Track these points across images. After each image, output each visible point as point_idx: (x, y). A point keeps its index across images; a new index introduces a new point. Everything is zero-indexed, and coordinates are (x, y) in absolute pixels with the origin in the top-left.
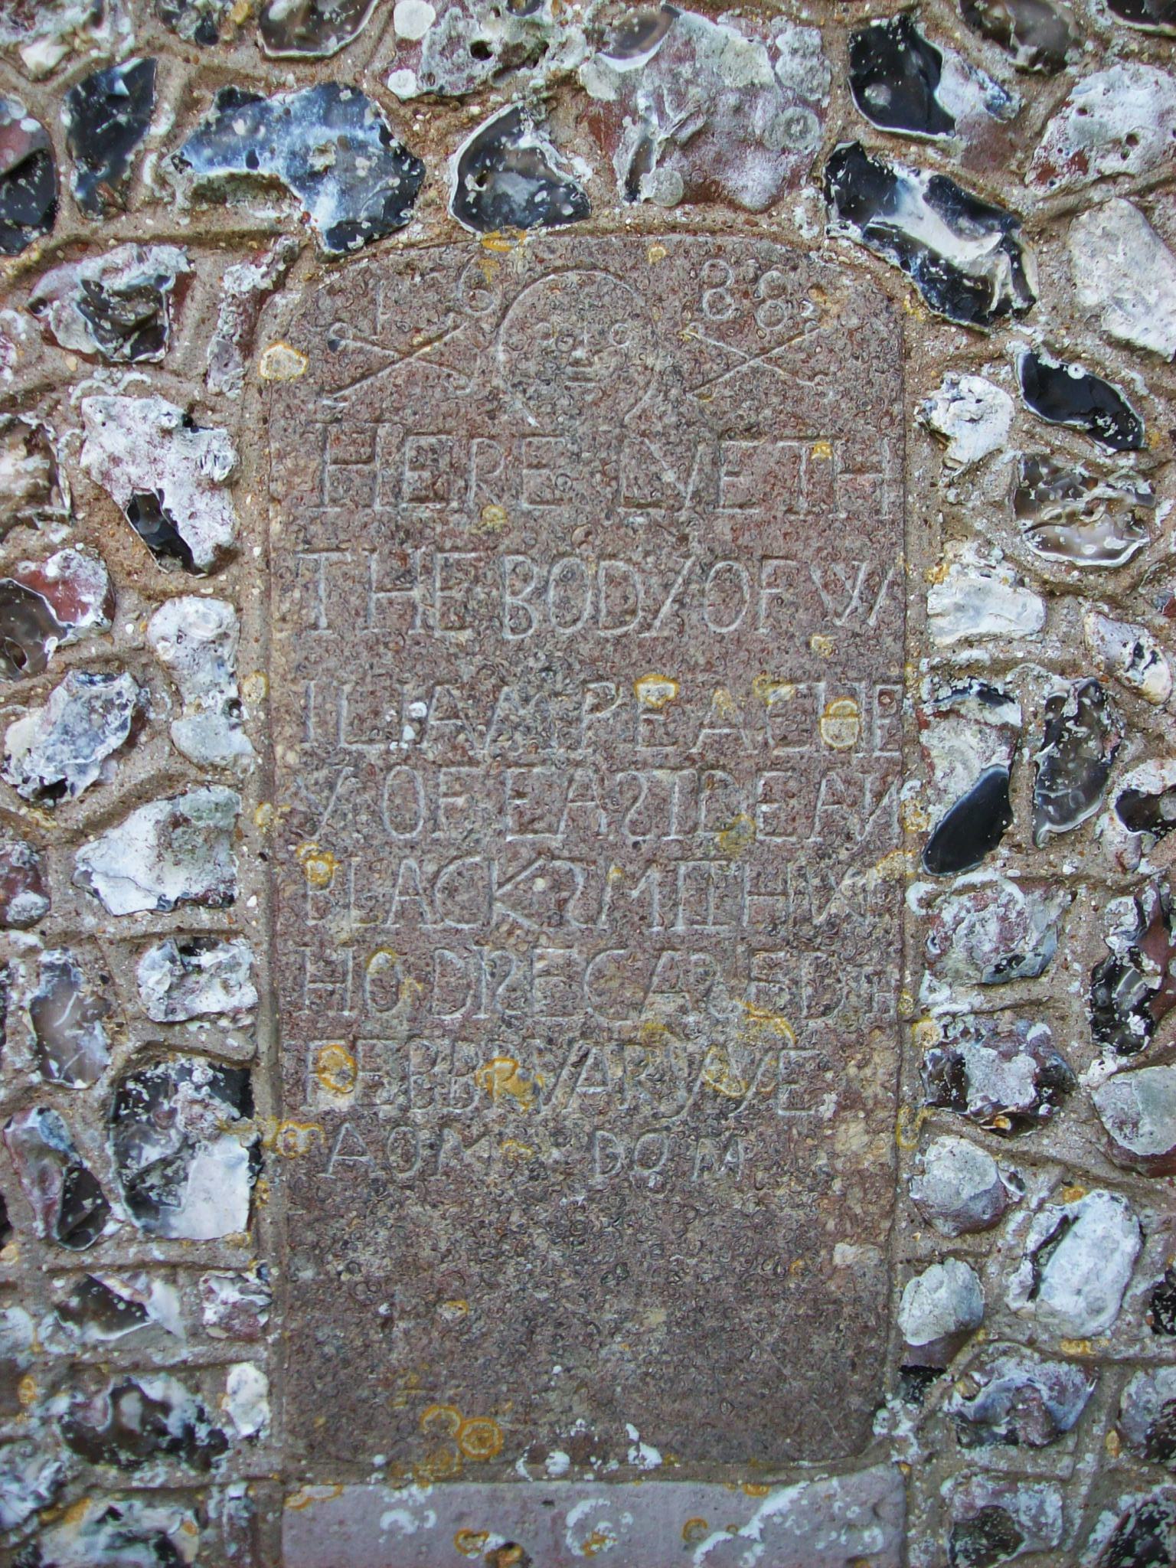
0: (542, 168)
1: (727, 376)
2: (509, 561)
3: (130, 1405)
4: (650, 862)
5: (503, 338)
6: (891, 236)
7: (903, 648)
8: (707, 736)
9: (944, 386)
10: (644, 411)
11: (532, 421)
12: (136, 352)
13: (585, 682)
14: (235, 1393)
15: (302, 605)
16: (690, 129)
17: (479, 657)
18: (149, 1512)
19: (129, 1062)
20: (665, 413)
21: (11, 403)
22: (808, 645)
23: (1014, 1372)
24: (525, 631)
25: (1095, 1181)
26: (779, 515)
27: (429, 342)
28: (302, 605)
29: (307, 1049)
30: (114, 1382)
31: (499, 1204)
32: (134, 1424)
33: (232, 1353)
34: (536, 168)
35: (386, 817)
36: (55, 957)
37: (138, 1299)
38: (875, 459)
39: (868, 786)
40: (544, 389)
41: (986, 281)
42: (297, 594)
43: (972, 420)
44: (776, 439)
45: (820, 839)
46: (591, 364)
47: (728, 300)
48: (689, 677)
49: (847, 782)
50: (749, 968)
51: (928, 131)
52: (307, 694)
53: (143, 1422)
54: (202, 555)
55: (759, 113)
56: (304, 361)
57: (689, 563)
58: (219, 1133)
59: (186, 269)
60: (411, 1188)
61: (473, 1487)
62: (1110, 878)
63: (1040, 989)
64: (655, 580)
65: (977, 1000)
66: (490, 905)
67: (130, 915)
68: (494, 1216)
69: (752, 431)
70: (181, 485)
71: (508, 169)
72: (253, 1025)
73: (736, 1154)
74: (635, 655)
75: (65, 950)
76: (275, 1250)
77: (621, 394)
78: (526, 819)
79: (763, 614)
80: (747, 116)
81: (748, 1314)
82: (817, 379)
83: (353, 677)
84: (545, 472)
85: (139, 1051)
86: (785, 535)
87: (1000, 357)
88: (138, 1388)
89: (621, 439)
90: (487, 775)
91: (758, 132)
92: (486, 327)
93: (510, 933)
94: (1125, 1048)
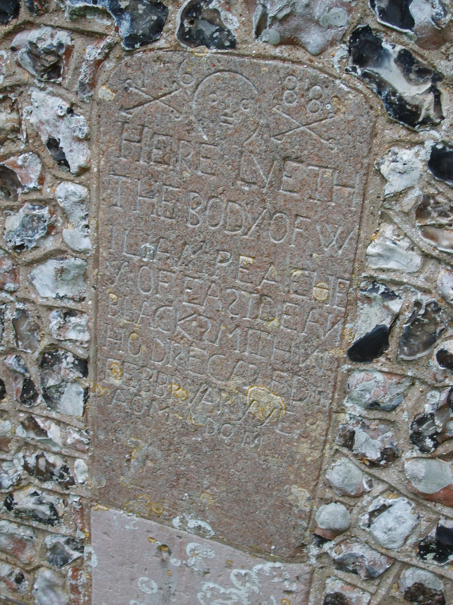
0: (218, 20)
1: (290, 132)
2: (193, 195)
3: (42, 462)
4: (237, 326)
5: (195, 98)
6: (375, 78)
7: (353, 266)
8: (265, 283)
9: (390, 154)
10: (252, 142)
11: (205, 137)
12: (49, 79)
13: (218, 250)
14: (77, 468)
15: (110, 196)
16: (285, 12)
17: (177, 231)
18: (48, 496)
19: (46, 348)
20: (261, 144)
21: (3, 90)
22: (311, 255)
23: (357, 549)
24: (196, 224)
25: (400, 494)
26: (306, 199)
27: (165, 95)
28: (110, 196)
29: (107, 361)
30: (38, 452)
31: (170, 433)
32: (43, 469)
33: (77, 455)
34: (215, 20)
35: (139, 284)
36: (20, 306)
37: (45, 429)
38: (351, 182)
39: (329, 318)
40: (211, 125)
41: (418, 108)
42: (109, 191)
43: (400, 173)
44: (309, 165)
45: (306, 335)
46: (232, 117)
47: (295, 96)
48: (260, 258)
49: (320, 315)
50: (272, 375)
51: (401, 27)
52: (112, 231)
53: (46, 468)
54: (74, 168)
55: (318, 8)
56: (114, 94)
57: (265, 211)
58: (75, 381)
59: (70, 43)
60: (139, 418)
61: (154, 523)
62: (430, 381)
63: (391, 416)
64: (249, 215)
65: (364, 413)
66: (175, 326)
67: (47, 298)
68: (168, 437)
69: (298, 160)
70: (67, 138)
71: (203, 19)
72: (88, 347)
73: (259, 441)
74: (238, 244)
75: (25, 304)
76: (92, 425)
77: (243, 133)
78: (191, 298)
79: (294, 239)
80: (312, 9)
81: (257, 498)
82: (330, 141)
83: (129, 228)
84: (209, 161)
85: (49, 345)
86: (307, 208)
87: (422, 143)
88: (45, 457)
89: (242, 152)
90: (177, 278)
91: (316, 18)
92: (189, 93)
93: (182, 338)
94: (423, 450)
